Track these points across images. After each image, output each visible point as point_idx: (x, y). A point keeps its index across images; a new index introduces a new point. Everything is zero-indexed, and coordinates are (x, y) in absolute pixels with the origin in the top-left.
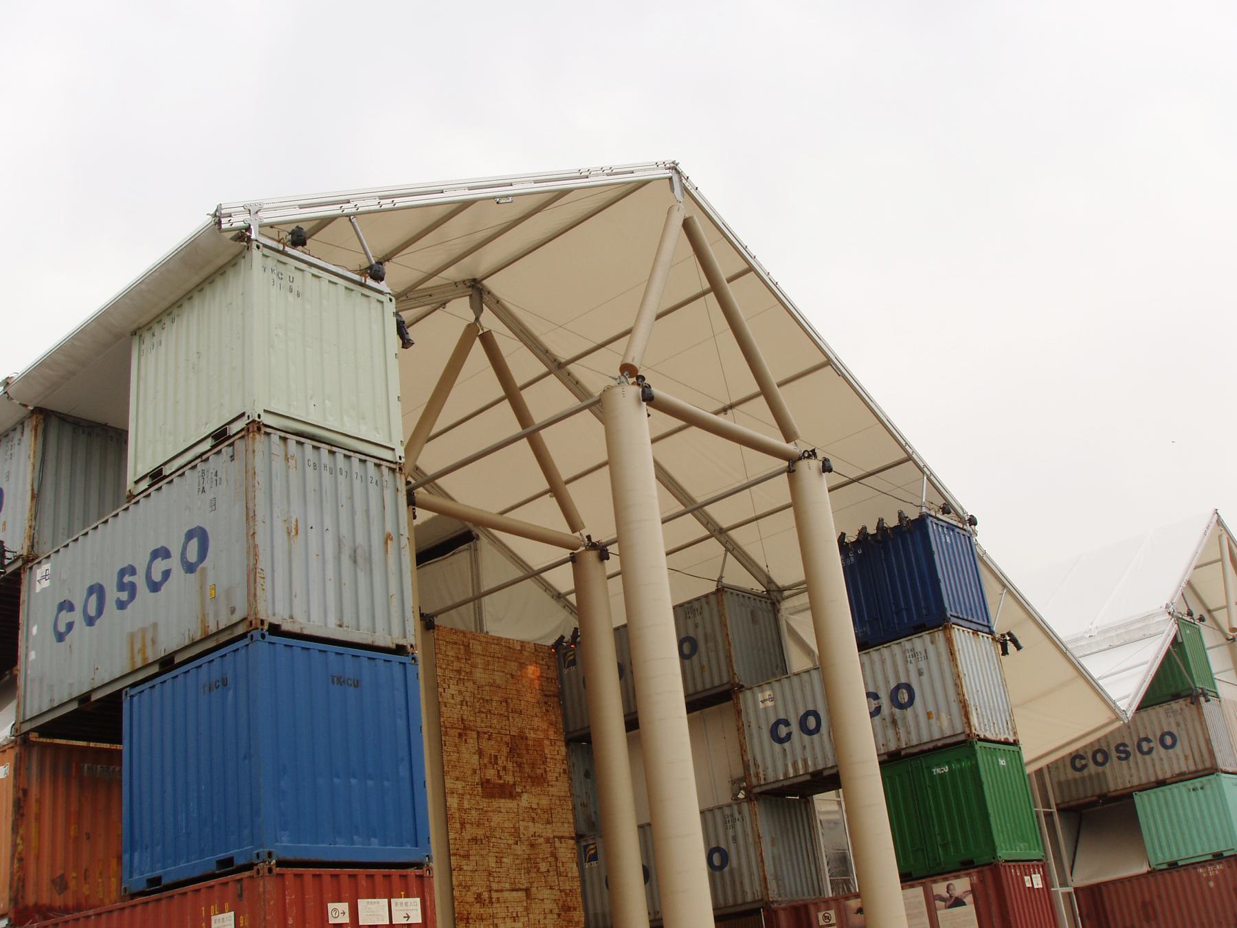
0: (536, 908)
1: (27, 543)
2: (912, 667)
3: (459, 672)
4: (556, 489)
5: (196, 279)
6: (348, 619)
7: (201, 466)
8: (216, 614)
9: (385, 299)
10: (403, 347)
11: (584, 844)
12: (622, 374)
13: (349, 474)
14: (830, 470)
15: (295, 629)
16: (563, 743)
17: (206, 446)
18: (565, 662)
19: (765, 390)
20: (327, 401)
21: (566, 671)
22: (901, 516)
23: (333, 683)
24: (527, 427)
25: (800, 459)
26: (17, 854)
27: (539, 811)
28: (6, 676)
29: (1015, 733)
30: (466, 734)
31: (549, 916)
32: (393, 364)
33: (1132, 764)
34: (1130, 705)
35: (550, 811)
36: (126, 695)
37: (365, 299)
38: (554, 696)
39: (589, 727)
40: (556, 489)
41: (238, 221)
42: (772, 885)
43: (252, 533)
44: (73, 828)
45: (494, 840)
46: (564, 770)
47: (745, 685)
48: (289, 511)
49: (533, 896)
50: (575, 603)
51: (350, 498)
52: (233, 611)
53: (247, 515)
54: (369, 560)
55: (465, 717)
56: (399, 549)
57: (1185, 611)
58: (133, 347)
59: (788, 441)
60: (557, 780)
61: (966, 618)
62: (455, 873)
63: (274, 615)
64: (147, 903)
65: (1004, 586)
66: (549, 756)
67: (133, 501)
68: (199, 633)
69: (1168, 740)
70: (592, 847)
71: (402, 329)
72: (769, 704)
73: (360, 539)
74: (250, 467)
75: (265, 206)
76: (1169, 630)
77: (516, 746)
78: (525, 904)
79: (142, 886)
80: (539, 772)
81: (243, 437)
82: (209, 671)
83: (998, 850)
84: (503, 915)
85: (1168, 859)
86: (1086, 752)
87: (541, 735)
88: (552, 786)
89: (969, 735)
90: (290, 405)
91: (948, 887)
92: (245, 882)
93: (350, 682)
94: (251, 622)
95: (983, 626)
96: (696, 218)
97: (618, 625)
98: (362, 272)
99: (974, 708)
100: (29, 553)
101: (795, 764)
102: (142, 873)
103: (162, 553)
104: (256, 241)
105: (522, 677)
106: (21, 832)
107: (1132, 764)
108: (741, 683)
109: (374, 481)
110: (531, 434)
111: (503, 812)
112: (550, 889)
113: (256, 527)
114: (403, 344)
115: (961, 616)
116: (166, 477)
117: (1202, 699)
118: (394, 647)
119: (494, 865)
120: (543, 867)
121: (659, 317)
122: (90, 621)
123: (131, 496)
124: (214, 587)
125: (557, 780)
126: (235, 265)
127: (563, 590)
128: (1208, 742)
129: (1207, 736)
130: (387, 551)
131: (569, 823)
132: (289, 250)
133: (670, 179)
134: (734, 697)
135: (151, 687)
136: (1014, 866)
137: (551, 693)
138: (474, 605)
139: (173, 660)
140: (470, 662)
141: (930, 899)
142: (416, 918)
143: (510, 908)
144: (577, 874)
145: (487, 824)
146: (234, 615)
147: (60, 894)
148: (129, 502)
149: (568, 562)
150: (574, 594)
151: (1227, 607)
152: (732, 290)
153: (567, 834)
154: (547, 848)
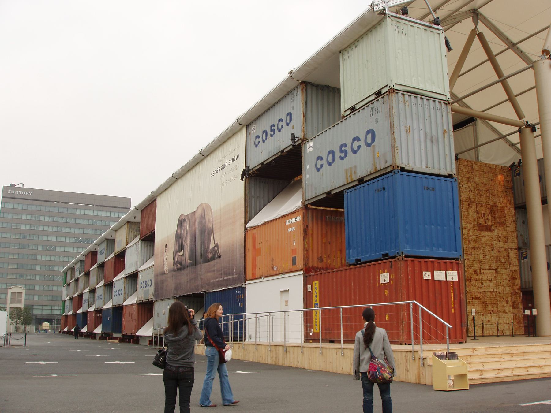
0: (499, 277)
1: (303, 134)
3: (468, 178)
4: (511, 99)
5: (364, 31)
6: (430, 165)
8: (380, 163)
9: (440, 32)
13: (429, 106)
15: (410, 169)
16: (513, 209)
17: (373, 97)
18: (515, 174)
20: (419, 78)
21: (515, 178)
23: (425, 189)
26: (305, 248)
27: (502, 237)
28: (292, 181)
30: (471, 204)
31: (505, 281)
32: (445, 60)
35: (507, 237)
36: (345, 192)
37: (432, 33)
38: (510, 188)
40: (511, 99)
41: (380, 7)
44: (324, 240)
45: (482, 248)
46: (514, 221)
48: (406, 123)
49: (498, 272)
50: (520, 148)
51: (429, 116)
52: (386, 162)
54: (438, 141)
55: (471, 197)
56: (449, 136)
58: (340, 58)
60: (510, 224)
62: (466, 261)
64: (355, 268)
66: (507, 214)
68: (373, 170)
70: (525, 253)
73: (434, 133)
77: (493, 209)
78: (495, 275)
79: (354, 262)
81: (387, 94)
82: (378, 184)
84: (486, 279)
87: (504, 205)
88: (508, 227)
90: (405, 80)
92: (393, 263)
94: (394, 166)
97: (539, 158)
98: (432, 22)
100: (304, 138)
102: (353, 257)
103: (357, 139)
104: (388, 14)
105: (496, 180)
109: (439, 109)
110: (503, 81)
111: (486, 237)
112: (506, 270)
113: (394, 130)
114: (448, 50)
116: (357, 110)
118: (448, 175)
119: (482, 258)
120: (503, 260)
122: (330, 164)
123: (343, 117)
124: (378, 153)
125: (510, 224)
127: (514, 142)
135: (355, 190)
137: (509, 187)
138: (475, 151)
140: (473, 174)
142: (456, 279)
143: (488, 277)
144: (517, 264)
145: (480, 242)
146: (387, 164)
147: (320, 263)
148: (343, 119)
149: (517, 132)
150: (520, 144)
153: (514, 247)
154: (505, 253)
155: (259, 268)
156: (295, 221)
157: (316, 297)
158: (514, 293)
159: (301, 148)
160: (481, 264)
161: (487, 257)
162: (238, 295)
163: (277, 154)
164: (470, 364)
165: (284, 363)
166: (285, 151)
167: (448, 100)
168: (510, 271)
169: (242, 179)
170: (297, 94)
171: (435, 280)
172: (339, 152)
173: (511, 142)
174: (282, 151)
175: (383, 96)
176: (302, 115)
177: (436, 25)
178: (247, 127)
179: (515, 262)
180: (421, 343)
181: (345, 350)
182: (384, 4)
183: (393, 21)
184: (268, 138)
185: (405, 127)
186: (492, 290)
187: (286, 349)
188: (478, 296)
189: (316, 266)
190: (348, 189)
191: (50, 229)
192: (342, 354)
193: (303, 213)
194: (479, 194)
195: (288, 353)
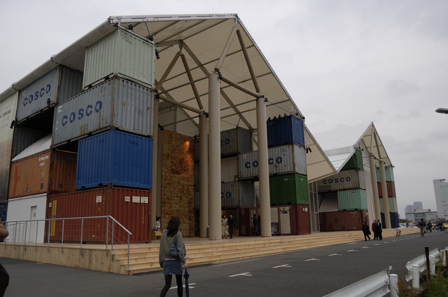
1: (56, 100)
2: (282, 153)
3: (168, 141)
4: (197, 97)
5: (103, 36)
6: (136, 128)
7: (101, 85)
8: (103, 123)
9: (153, 46)
10: (157, 59)
11: (196, 187)
12: (215, 70)
13: (139, 91)
14: (267, 101)
15: (122, 129)
16: (194, 162)
17: (103, 80)
19: (253, 78)
21: (196, 144)
22: (285, 115)
24: (191, 81)
25: (260, 97)
29: (306, 173)
31: (186, 204)
33: (338, 184)
34: (339, 169)
37: (148, 45)
39: (199, 159)
40: (197, 97)
41: (115, 21)
42: (241, 203)
43: (113, 104)
45: (173, 184)
47: (241, 153)
52: (107, 123)
53: (112, 99)
54: (143, 113)
55: (169, 153)
56: (151, 111)
57: (358, 147)
59: (257, 93)
61: (298, 142)
62: (163, 191)
63: (117, 125)
64: (81, 192)
65: (310, 135)
66: (190, 165)
67: (84, 92)
68: (98, 128)
69: (348, 179)
70: (198, 188)
71: (157, 53)
72: (246, 158)
73: (141, 108)
74: (114, 87)
75: (123, 18)
76: (353, 151)
78: (180, 201)
79: (80, 188)
81: (112, 79)
83: (297, 201)
85: (344, 208)
86: (327, 179)
88: (189, 172)
89: (294, 172)
91: (284, 208)
93: (135, 143)
94: (111, 127)
95: (302, 145)
96: (240, 30)
99: (296, 166)
100: (57, 103)
101: (250, 174)
103: (90, 106)
106: (51, 172)
107: (338, 184)
108: (240, 152)
110: (192, 83)
112: (186, 197)
115: (297, 142)
117: (359, 170)
118: (147, 136)
120: (185, 192)
122: (71, 122)
124: (103, 117)
125: (191, 171)
126: (113, 33)
128: (358, 181)
129: (358, 179)
130: (148, 112)
131: (193, 182)
132: (128, 30)
133: (235, 19)
134: (237, 155)
136: (301, 205)
138: (174, 125)
139: (91, 134)
141: (279, 211)
142: (147, 202)
147: (60, 188)
148: (83, 92)
151: (370, 147)
152: (248, 51)
153: (192, 185)
154: (187, 187)
155: (18, 190)
156: (45, 159)
157: (54, 211)
158: (190, 212)
159: (54, 110)
160: (172, 194)
161: (175, 189)
162: (2, 208)
163: (38, 112)
164: (145, 258)
165: (24, 258)
166: (43, 110)
167: (153, 88)
168: (189, 198)
169: (11, 127)
170: (55, 72)
171: (133, 202)
172: (78, 114)
173: (196, 123)
174: (42, 110)
175: (109, 80)
176: (57, 87)
177: (151, 40)
178: (20, 92)
179: (192, 193)
180: (129, 243)
181: (64, 249)
182: (117, 20)
183: (123, 32)
184: (33, 100)
185: (122, 102)
186: (177, 209)
187: (26, 248)
188: (169, 213)
189: (57, 190)
190: (81, 139)
192: (62, 251)
193: (51, 153)
194: (174, 151)
195: (27, 251)
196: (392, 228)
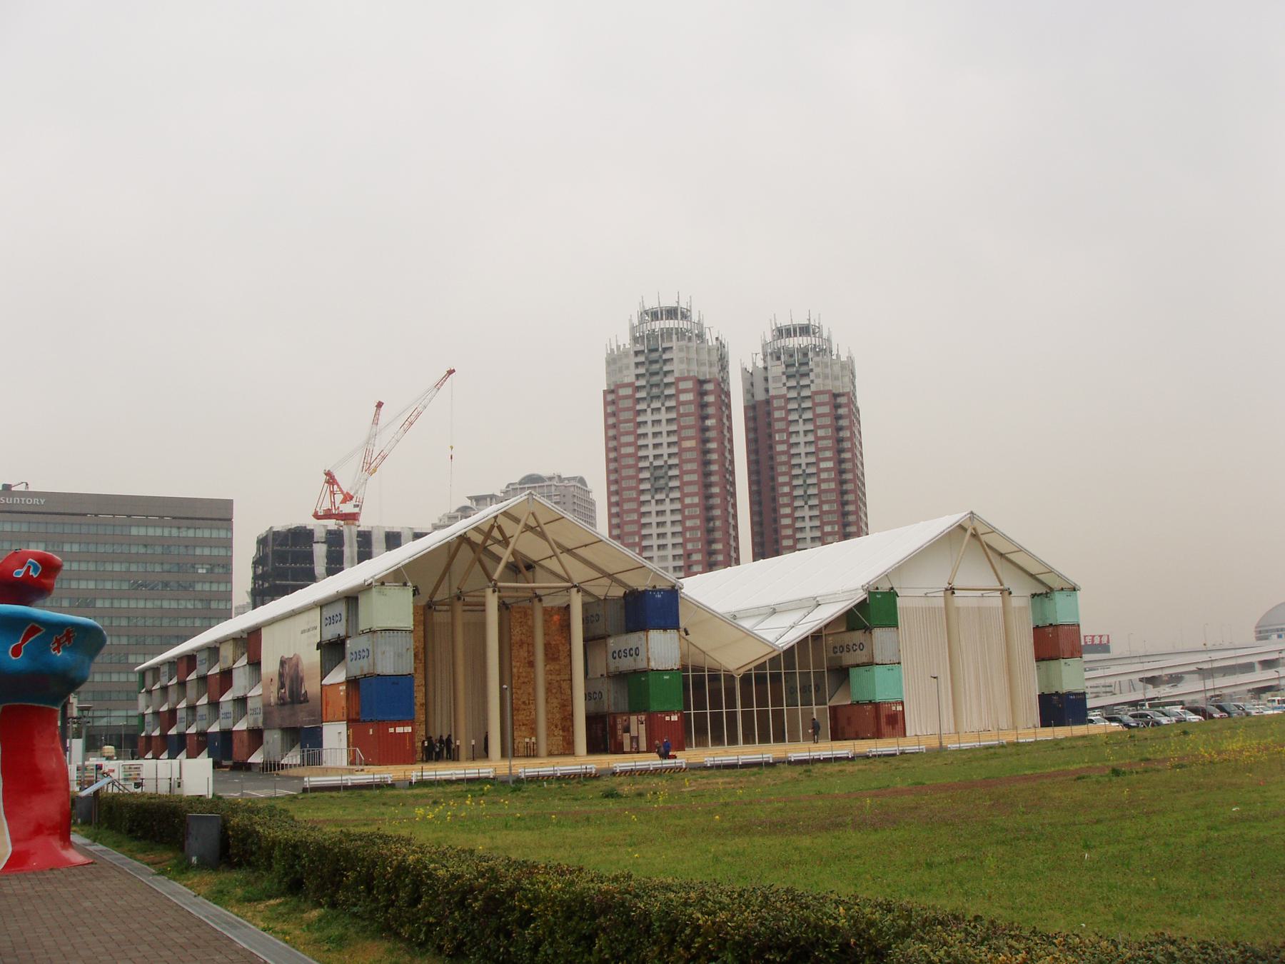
3: (521, 622)
80: (555, 656)
87: (558, 642)
120: (554, 691)
121: (512, 537)
142: (410, 730)
154: (556, 684)
191: (84, 567)
196: (1041, 726)
